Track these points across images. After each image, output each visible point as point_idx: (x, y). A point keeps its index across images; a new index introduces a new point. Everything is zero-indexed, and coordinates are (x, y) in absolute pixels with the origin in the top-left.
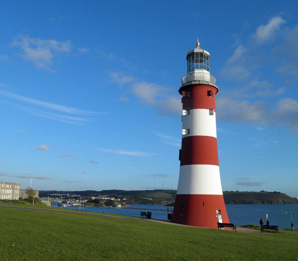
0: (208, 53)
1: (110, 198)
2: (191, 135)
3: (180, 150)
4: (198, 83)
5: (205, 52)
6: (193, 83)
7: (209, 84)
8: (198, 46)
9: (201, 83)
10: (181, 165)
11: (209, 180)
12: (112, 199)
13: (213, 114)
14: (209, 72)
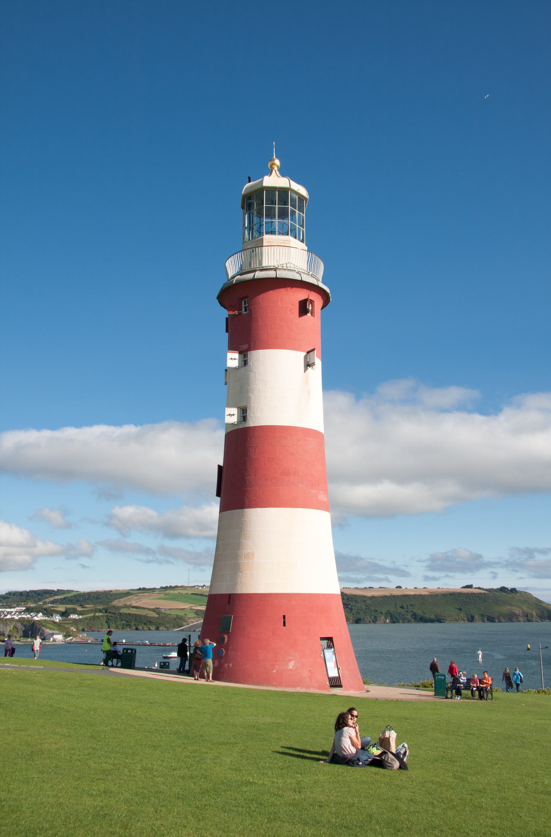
0: (303, 192)
1: (29, 614)
2: (248, 426)
3: (219, 466)
4: (271, 274)
5: (295, 186)
6: (259, 275)
7: (304, 279)
8: (276, 168)
9: (281, 274)
10: (223, 508)
11: (295, 554)
12: (36, 618)
13: (313, 364)
14: (306, 245)
